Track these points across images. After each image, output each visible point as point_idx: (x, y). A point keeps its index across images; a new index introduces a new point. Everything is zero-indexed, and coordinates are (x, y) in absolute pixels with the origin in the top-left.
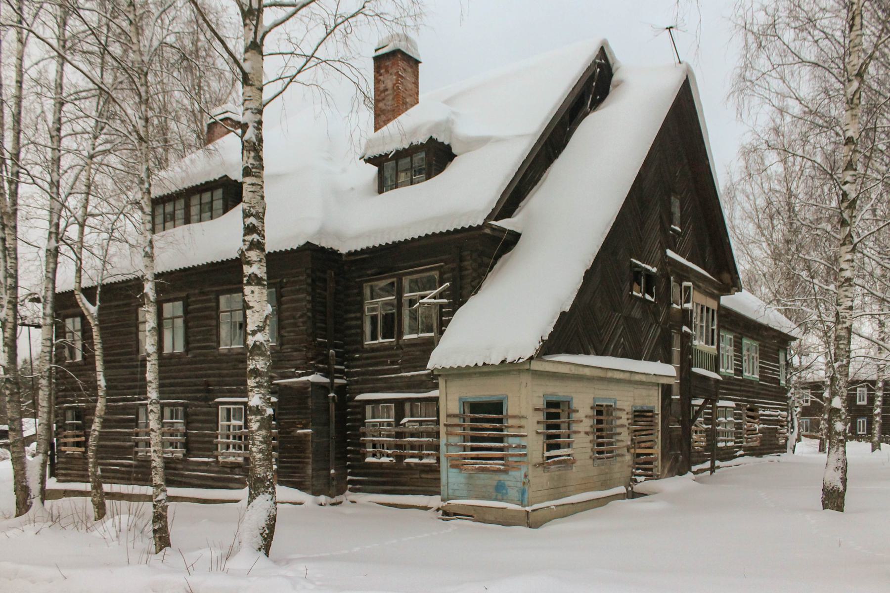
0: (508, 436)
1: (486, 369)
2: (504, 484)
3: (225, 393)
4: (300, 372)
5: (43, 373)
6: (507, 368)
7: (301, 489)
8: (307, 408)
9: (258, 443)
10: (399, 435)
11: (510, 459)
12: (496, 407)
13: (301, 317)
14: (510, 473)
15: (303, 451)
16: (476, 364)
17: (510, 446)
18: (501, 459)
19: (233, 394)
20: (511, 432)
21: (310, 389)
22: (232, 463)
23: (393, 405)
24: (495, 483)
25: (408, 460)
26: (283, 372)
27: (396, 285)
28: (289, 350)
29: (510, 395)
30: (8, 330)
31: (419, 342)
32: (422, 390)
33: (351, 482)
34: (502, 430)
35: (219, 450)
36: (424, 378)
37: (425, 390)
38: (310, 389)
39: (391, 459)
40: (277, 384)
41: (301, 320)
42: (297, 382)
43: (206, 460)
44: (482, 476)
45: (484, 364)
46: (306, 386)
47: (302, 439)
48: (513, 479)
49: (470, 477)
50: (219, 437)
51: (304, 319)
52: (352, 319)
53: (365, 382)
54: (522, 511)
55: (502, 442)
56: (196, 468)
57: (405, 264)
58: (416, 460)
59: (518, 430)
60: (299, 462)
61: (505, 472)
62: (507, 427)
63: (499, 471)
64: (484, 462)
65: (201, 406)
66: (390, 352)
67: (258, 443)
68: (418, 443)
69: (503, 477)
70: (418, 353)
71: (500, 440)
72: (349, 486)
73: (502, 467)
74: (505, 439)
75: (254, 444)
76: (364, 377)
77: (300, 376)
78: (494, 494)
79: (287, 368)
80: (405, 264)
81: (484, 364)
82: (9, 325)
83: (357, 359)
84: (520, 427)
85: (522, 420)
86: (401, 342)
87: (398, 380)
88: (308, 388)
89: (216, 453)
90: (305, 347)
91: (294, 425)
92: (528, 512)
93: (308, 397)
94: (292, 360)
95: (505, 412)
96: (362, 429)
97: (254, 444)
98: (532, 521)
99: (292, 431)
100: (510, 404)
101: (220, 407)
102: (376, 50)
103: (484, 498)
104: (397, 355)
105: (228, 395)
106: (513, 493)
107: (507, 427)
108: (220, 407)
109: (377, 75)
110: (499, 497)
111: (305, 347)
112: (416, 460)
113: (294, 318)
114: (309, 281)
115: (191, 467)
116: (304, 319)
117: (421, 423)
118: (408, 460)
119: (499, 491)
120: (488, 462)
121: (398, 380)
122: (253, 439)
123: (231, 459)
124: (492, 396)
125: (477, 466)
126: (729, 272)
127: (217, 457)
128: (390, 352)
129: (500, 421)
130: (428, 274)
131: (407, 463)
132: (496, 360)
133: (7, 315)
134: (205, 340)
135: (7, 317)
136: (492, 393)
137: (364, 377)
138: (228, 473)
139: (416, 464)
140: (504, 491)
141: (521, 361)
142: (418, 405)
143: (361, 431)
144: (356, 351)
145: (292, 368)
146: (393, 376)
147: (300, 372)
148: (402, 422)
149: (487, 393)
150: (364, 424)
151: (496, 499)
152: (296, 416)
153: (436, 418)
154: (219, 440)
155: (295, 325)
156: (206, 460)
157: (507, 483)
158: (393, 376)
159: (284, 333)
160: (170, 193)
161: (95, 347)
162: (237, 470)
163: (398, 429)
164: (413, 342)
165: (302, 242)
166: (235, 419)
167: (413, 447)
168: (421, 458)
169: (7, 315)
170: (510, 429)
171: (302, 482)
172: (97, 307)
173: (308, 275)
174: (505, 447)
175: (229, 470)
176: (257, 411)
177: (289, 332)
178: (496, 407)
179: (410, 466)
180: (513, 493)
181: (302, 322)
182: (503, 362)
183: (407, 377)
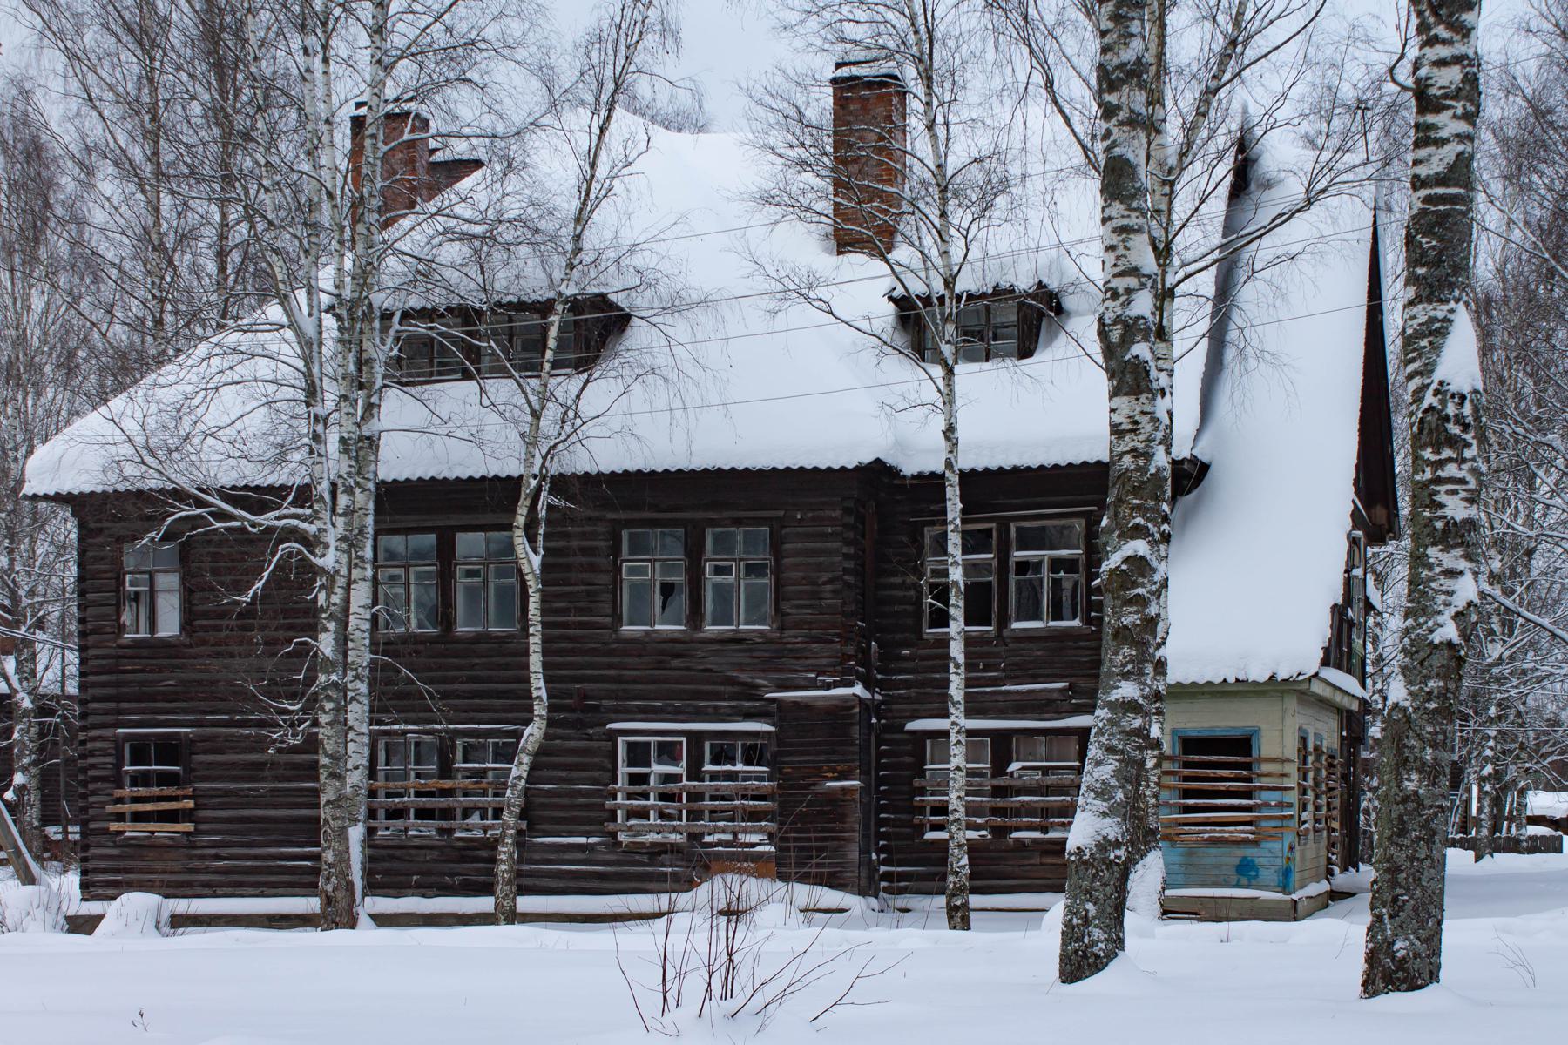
0: (1262, 788)
1: (1241, 688)
2: (1252, 861)
3: (635, 713)
4: (829, 679)
5: (360, 670)
6: (1276, 688)
7: (832, 887)
8: (852, 743)
9: (1152, 785)
10: (998, 791)
11: (1264, 824)
12: (1241, 745)
13: (830, 581)
14: (1263, 845)
15: (842, 818)
16: (1225, 680)
17: (1267, 805)
18: (1249, 823)
19: (650, 716)
20: (1265, 782)
21: (857, 710)
22: (654, 844)
23: (684, 739)
24: (1236, 861)
25: (1016, 835)
26: (787, 679)
27: (995, 534)
28: (799, 639)
29: (1263, 727)
30: (337, 590)
31: (1044, 634)
32: (1047, 716)
33: (887, 876)
34: (1249, 780)
35: (619, 821)
36: (1055, 696)
37: (1055, 716)
38: (857, 710)
39: (984, 833)
40: (774, 700)
41: (829, 587)
42: (824, 697)
43: (583, 840)
44: (1213, 851)
45: (1237, 680)
46: (849, 704)
47: (836, 801)
48: (1269, 855)
49: (1190, 853)
50: (619, 795)
51: (838, 586)
52: (894, 587)
53: (921, 699)
54: (1286, 901)
55: (1250, 798)
56: (552, 857)
57: (1014, 501)
58: (1037, 835)
59: (1280, 780)
60: (834, 839)
61: (1256, 843)
62: (1259, 775)
63: (1245, 842)
64: (1218, 828)
65: (569, 738)
66: (985, 649)
67: (1152, 785)
68: (1042, 805)
69: (1249, 852)
70: (1039, 653)
71: (1247, 794)
72: (883, 884)
73: (1251, 836)
74: (1256, 794)
75: (1147, 786)
76: (922, 691)
77: (828, 686)
78: (1234, 878)
79: (796, 671)
80: (1014, 501)
81: (1237, 680)
82: (341, 582)
83: (905, 658)
84: (1283, 775)
85: (1286, 764)
86: (1006, 633)
87: (1000, 698)
88: (853, 707)
89: (611, 827)
90: (839, 635)
91: (820, 774)
92: (1295, 902)
93: (852, 724)
94: (807, 658)
95: (1255, 754)
96: (917, 782)
97: (1147, 786)
98: (1293, 913)
99: (814, 784)
100: (1264, 740)
101: (620, 739)
102: (838, 66)
103: (1216, 885)
104: (997, 655)
105: (639, 716)
106: (1268, 875)
107: (1259, 775)
108: (620, 739)
109: (841, 112)
110: (1244, 881)
111: (839, 635)
112: (1037, 835)
113: (814, 583)
114: (851, 520)
115: (537, 856)
116: (838, 586)
117: (1045, 771)
118: (1016, 835)
119: (1246, 872)
120: (1226, 828)
121: (1000, 698)
122: (1147, 780)
123: (652, 837)
124: (1234, 728)
125: (1206, 836)
126: (1387, 507)
127: (614, 835)
128: (985, 649)
129: (1247, 766)
130: (1063, 522)
131: (1017, 840)
132: (1259, 674)
133: (337, 562)
134: (590, 612)
135: (337, 566)
136: (1232, 724)
137: (922, 691)
138: (643, 864)
139: (1034, 840)
140: (1253, 873)
141: (1301, 678)
142: (1041, 742)
143: (916, 785)
144: (907, 645)
145: (811, 671)
146: (988, 689)
147: (829, 679)
148: (1010, 769)
149: (1223, 724)
150: (922, 774)
151: (1238, 885)
152: (822, 758)
153: (1077, 763)
154: (652, 801)
155: (816, 595)
156: (583, 840)
157: (1257, 861)
158: (988, 689)
159: (786, 607)
160: (429, 306)
161: (531, 630)
162: (666, 858)
163: (996, 782)
164: (1031, 634)
165: (867, 458)
166: (659, 762)
167: (1030, 810)
168: (1045, 830)
169: (337, 562)
170: (1264, 779)
171: (836, 872)
172: (540, 558)
173: (847, 511)
174: (1257, 805)
175: (645, 859)
176: (1157, 744)
177: (798, 607)
178: (1241, 745)
179: (1024, 844)
180: (1268, 875)
181: (833, 592)
182: (1272, 677)
183: (1018, 693)
